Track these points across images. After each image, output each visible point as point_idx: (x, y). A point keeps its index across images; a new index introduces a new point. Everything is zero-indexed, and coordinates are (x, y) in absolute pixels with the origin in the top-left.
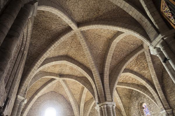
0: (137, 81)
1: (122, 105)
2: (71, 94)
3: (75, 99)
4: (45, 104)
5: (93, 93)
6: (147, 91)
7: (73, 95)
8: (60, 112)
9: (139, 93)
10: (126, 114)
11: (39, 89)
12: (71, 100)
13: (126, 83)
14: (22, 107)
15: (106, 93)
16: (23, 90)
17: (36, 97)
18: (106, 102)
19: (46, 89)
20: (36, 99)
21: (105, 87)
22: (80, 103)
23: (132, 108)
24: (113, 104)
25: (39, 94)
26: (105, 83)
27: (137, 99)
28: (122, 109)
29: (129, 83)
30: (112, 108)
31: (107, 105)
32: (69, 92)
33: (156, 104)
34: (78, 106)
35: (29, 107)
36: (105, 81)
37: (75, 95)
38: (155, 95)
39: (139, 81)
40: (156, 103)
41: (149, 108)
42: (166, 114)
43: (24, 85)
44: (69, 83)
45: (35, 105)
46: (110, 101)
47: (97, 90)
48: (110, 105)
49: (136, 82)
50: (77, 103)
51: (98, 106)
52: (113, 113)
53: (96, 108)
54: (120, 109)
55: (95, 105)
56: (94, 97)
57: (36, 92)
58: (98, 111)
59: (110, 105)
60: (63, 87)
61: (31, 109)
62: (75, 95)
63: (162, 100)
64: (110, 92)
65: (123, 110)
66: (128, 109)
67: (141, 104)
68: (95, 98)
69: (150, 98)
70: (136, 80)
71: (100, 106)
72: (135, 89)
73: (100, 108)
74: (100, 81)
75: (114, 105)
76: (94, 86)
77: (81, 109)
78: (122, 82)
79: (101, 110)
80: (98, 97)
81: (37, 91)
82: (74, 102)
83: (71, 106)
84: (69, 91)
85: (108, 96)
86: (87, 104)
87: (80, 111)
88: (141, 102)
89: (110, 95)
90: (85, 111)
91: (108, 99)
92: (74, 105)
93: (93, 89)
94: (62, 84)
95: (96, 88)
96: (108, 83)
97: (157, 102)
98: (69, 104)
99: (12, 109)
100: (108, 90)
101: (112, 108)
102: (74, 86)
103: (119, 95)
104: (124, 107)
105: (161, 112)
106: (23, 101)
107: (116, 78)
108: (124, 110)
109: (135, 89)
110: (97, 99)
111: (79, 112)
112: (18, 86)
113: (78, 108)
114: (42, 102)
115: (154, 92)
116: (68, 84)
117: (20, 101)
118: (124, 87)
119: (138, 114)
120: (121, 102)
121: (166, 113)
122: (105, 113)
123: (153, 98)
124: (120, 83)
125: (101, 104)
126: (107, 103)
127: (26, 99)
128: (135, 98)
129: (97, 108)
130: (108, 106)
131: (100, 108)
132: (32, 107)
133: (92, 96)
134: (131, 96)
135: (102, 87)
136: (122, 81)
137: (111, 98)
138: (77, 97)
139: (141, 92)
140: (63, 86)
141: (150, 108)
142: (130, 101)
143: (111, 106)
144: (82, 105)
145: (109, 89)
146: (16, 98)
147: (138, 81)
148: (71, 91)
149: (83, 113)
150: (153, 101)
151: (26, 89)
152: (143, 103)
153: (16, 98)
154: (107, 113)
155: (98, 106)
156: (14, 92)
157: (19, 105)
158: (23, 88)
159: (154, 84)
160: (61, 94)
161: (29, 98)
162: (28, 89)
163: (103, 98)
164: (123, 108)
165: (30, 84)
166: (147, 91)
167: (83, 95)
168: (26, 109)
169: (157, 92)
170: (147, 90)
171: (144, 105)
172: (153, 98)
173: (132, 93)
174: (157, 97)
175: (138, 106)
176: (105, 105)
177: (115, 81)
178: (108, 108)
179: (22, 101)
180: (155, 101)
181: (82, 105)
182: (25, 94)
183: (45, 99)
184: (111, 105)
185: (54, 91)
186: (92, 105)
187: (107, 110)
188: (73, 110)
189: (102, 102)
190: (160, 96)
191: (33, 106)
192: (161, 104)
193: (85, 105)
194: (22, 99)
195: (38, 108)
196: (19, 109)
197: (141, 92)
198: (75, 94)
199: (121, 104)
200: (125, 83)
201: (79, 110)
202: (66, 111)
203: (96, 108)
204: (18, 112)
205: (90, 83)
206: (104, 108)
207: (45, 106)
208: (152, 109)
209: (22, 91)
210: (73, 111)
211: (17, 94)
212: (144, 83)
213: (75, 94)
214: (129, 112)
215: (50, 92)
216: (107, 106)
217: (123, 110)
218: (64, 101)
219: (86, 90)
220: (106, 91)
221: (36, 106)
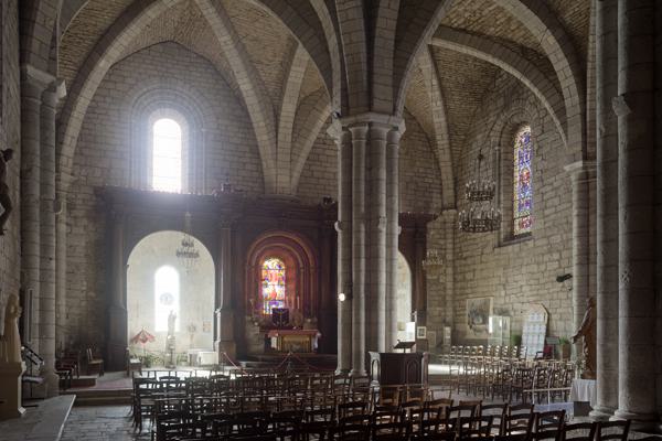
0: (523, 32)
1: (444, 124)
2: (244, 62)
3: (259, 84)
4: (145, 93)
5: (326, 71)
6: (550, 81)
7: (252, 65)
8: (203, 130)
9: (519, 82)
10: (452, 158)
11: (108, 31)
12: (245, 85)
13: (479, 34)
14: (55, 112)
15: (375, 78)
16: (42, 43)
17: (103, 65)
18: (367, 116)
19: (138, 31)
20: (104, 73)
21: (376, 51)
22: (281, 99)
23: (479, 137)
24: (395, 125)
25: (115, 52)
26: (377, 31)
27: (506, 106)
28: (438, 137)
29: (489, 37)
30: (390, 136)
31: (370, 124)
32: (235, 52)
33: (563, 138)
34: (272, 113)
35: (83, 102)
36: (380, 22)
37: (259, 67)
38: (572, 100)
39: (533, 32)
40: (566, 132)
41: (536, 148)
42: (581, 174)
43: (39, 18)
44: (237, 12)
45: (104, 97)
46: (384, 113)
47: (342, 61)
48: (382, 125)
49: (518, 37)
50: (269, 100)
51: (337, 124)
52: (387, 158)
53: (331, 131)
54: (434, 138)
55: (329, 122)
56: (330, 88)
57: (100, 40)
58: (336, 142)
59: (382, 125)
60: (210, 27)
61: (91, 110)
62: (259, 67)
63: (588, 125)
64: (391, 73)
65: (442, 140)
66: (465, 140)
67: (516, 128)
68: (331, 92)
69: (551, 112)
70: (520, 24)
71: (345, 125)
72: (506, 67)
73: (343, 133)
74: (361, 24)
75: (396, 129)
76: (332, 42)
77: (282, 124)
78: (463, 27)
79: (347, 142)
80: (344, 90)
81: (102, 36)
82: (257, 94)
83: (244, 109)
84: (236, 47)
85: (382, 91)
86: (306, 106)
87: (280, 130)
88: (516, 120)
89: (391, 89)
90: (298, 131)
91: (377, 104)
92: (257, 108)
93: (328, 53)
94: (205, 13)
95: (341, 51)
96: (392, 36)
97: (570, 129)
98: (239, 99)
99: (19, 119)
100: (384, 65)
101: (390, 136)
102: (257, 24)
103: (440, 80)
104: (451, 129)
105: (567, 168)
106: (52, 88)
107: (432, 12)
108: (446, 142)
109: (506, 67)
110: (338, 98)
111: (277, 136)
112: (16, 26)
113: (272, 118)
114: (131, 87)
115: (574, 88)
116: (231, 14)
117: (42, 89)
118: (465, 50)
119: (494, 161)
120: (442, 113)
121: (581, 171)
122: (358, 153)
123: (561, 112)
124: (446, 31)
125: (352, 119)
126: (372, 117)
127: (60, 80)
128: (501, 102)
129: (336, 132)
130: (373, 128)
131: (343, 133)
132: (94, 103)
133: (319, 78)
134: (487, 90)
135: (364, 49)
136: (462, 20)
137: (390, 98)
138: (270, 73)
139: (527, 83)
140: (211, 22)
141: (539, 147)
142: (479, 110)
143: (385, 131)
144: (288, 108)
145: (389, 63)
146: (23, 76)
147: (528, 35)
148: (244, 45)
149: (289, 138)
150: (558, 123)
151: (54, 39)
152: (524, 123)
153: (23, 76)
154: (366, 156)
155: (337, 124)
156: (7, 57)
157: (40, 103)
158: (39, 36)
159: (587, 54)
160: (205, 55)
161: (75, 64)
162: (60, 37)
163: (358, 99)
164: (446, 136)
165: (63, 14)
166: (550, 81)
167: (293, 68)
168: (71, 110)
169: (585, 97)
170: (551, 78)
171: (521, 137)
172: (561, 112)
173: (494, 77)
174: (579, 110)
175: (502, 133)
176: (363, 124)
177: (424, 27)
178: (372, 139)
179: (47, 90)
180: (564, 124)
181: (288, 108)
182: (55, 59)
183: (140, 74)
184: (387, 126)
185: (176, 40)
186: (321, 123)
187: (367, 144)
188: (251, 124)
189: (355, 115)
190: (588, 107)
191: (98, 98)
192: (580, 139)
193: (298, 109)
194: (47, 82)
195: (118, 110)
196: (44, 117)
197: (527, 83)
198: (262, 63)
199: (443, 119)
200: (473, 33)
201: (277, 127)
202: (227, 126)
203: (331, 131)
204: (44, 128)
205: (320, 23)
206: (358, 134)
207: (145, 103)
208: (544, 150)
209: (35, 45)
210: (253, 128)
211: (23, 60)
212: (549, 44)
213: (262, 63)
214: (464, 151)
215: (158, 46)
216: (370, 131)
217: (442, 140)
218: (217, 87)
219: (302, 54)
220: (375, 70)
221: (108, 100)
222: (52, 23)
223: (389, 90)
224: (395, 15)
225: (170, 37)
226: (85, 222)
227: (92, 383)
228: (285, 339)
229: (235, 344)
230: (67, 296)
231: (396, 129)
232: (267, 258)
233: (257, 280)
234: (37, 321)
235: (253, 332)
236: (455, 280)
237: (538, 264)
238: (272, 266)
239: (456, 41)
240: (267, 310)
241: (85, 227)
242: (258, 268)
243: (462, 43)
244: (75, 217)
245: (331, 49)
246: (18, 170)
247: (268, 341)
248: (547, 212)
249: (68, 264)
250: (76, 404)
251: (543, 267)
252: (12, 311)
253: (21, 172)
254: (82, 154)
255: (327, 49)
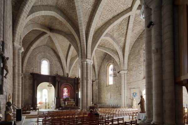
5: (77, 51)
17: (32, 48)
21: (88, 47)
25: (34, 46)
31: (87, 61)
43: (17, 32)
49: (111, 48)
56: (78, 54)
91: (88, 57)
106: (20, 49)
128: (107, 60)
130: (87, 62)
134: (104, 58)
145: (90, 50)
193: (70, 60)
205: (76, 41)
209: (16, 39)
216: (86, 63)
219: (72, 48)
222: (20, 34)
223: (90, 55)
224: (92, 40)
225: (45, 44)
226: (28, 80)
227: (30, 113)
228: (69, 103)
229: (58, 105)
230: (24, 95)
231: (91, 63)
232: (64, 88)
233: (63, 92)
234: (17, 100)
235: (62, 102)
236: (98, 93)
237: (114, 90)
238: (65, 90)
239: (100, 48)
240: (64, 97)
241: (28, 81)
242: (63, 90)
243: (101, 49)
244: (26, 79)
245: (79, 46)
246: (12, 66)
247: (65, 103)
248: (116, 80)
249: (25, 88)
250: (26, 118)
251: (115, 90)
252: (10, 97)
253: (13, 67)
254: (27, 66)
255: (78, 47)
